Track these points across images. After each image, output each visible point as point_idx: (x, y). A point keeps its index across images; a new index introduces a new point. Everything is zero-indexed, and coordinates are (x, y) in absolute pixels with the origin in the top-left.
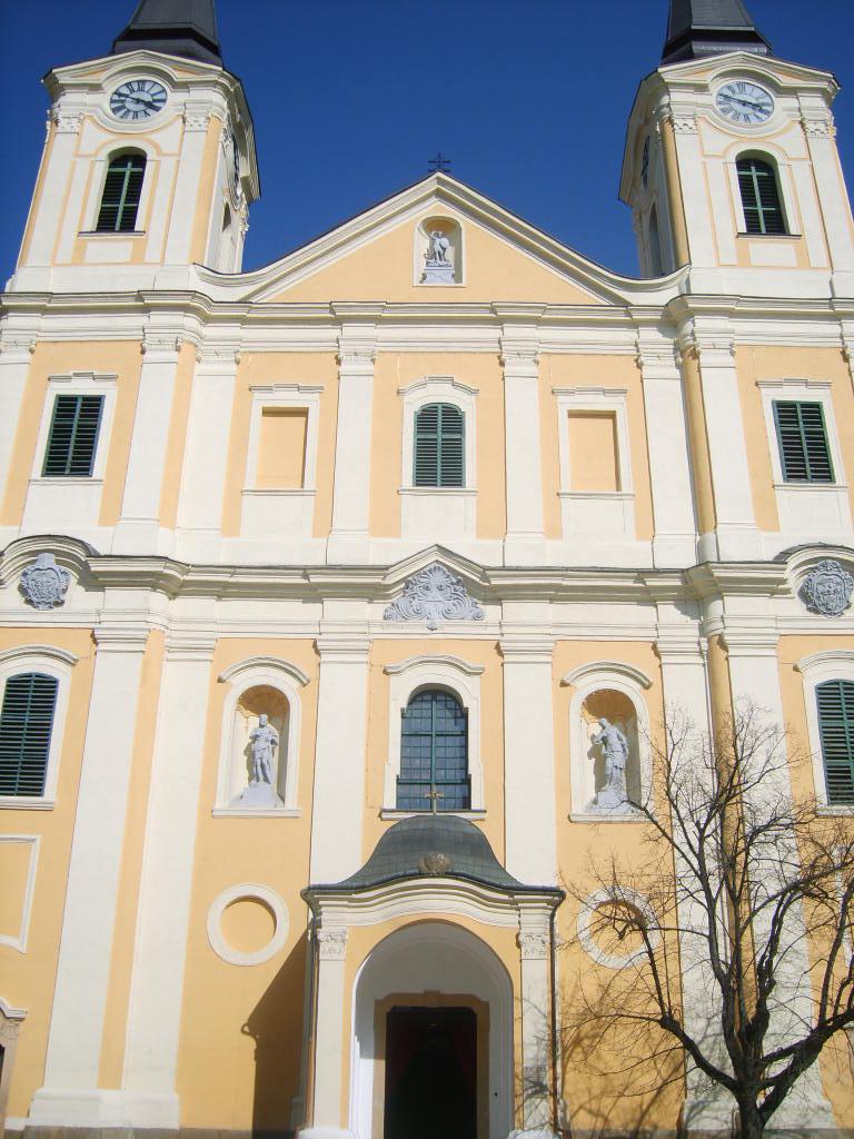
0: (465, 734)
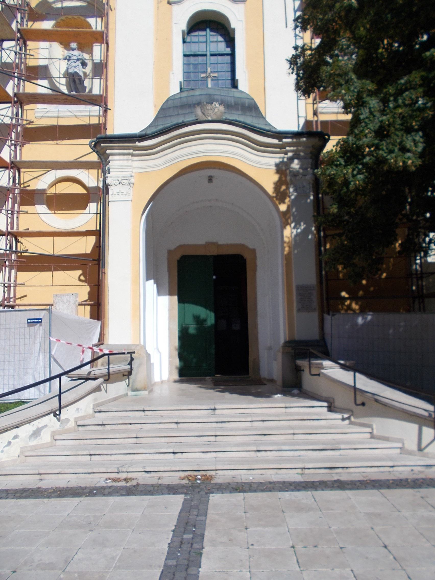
0: (233, 55)
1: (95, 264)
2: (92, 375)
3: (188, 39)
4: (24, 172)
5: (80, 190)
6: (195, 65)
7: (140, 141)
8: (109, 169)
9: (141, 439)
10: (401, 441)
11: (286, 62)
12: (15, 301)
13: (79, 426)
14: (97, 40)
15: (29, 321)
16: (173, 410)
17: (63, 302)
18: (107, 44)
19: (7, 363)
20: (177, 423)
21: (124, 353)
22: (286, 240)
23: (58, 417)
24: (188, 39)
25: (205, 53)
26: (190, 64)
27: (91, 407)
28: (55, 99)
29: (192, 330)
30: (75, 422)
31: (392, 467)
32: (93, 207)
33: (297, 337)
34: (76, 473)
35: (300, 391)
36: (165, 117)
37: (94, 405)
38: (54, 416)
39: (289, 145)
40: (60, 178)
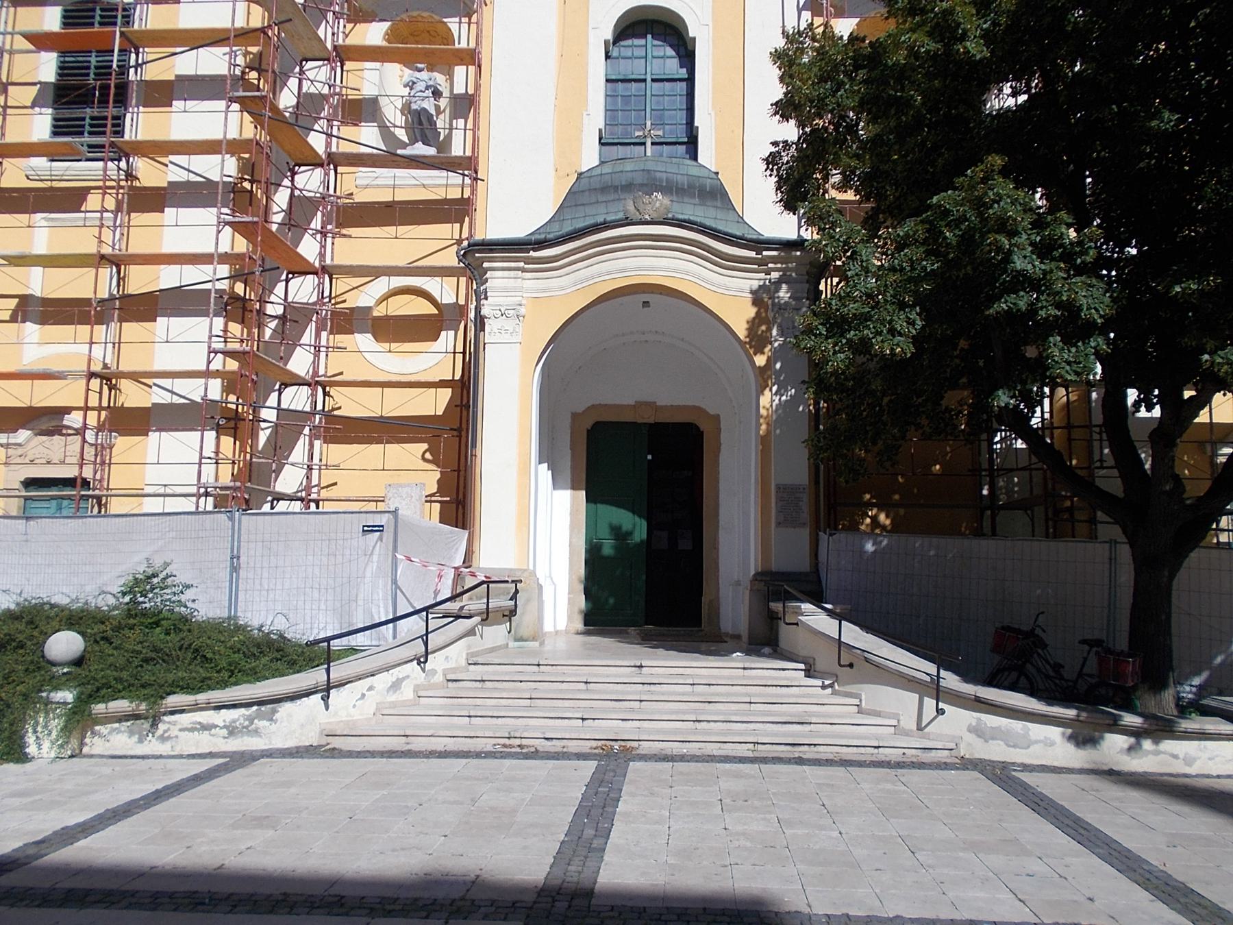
0: (690, 80)
1: (453, 436)
2: (465, 612)
3: (615, 52)
4: (337, 278)
5: (428, 309)
6: (626, 98)
7: (535, 250)
8: (486, 292)
9: (537, 701)
10: (896, 716)
11: (761, 161)
12: (319, 493)
13: (448, 680)
14: (462, 60)
15: (366, 528)
16: (558, 718)
17: (401, 496)
18: (480, 66)
19: (323, 591)
20: (586, 683)
21: (507, 582)
22: (763, 412)
23: (422, 665)
24: (615, 52)
25: (643, 77)
26: (617, 96)
27: (464, 656)
28: (393, 161)
29: (607, 550)
30: (414, 691)
32: (447, 339)
33: (774, 567)
34: (454, 737)
35: (775, 651)
36: (576, 205)
37: (467, 654)
38: (419, 664)
39: (774, 260)
40: (395, 288)
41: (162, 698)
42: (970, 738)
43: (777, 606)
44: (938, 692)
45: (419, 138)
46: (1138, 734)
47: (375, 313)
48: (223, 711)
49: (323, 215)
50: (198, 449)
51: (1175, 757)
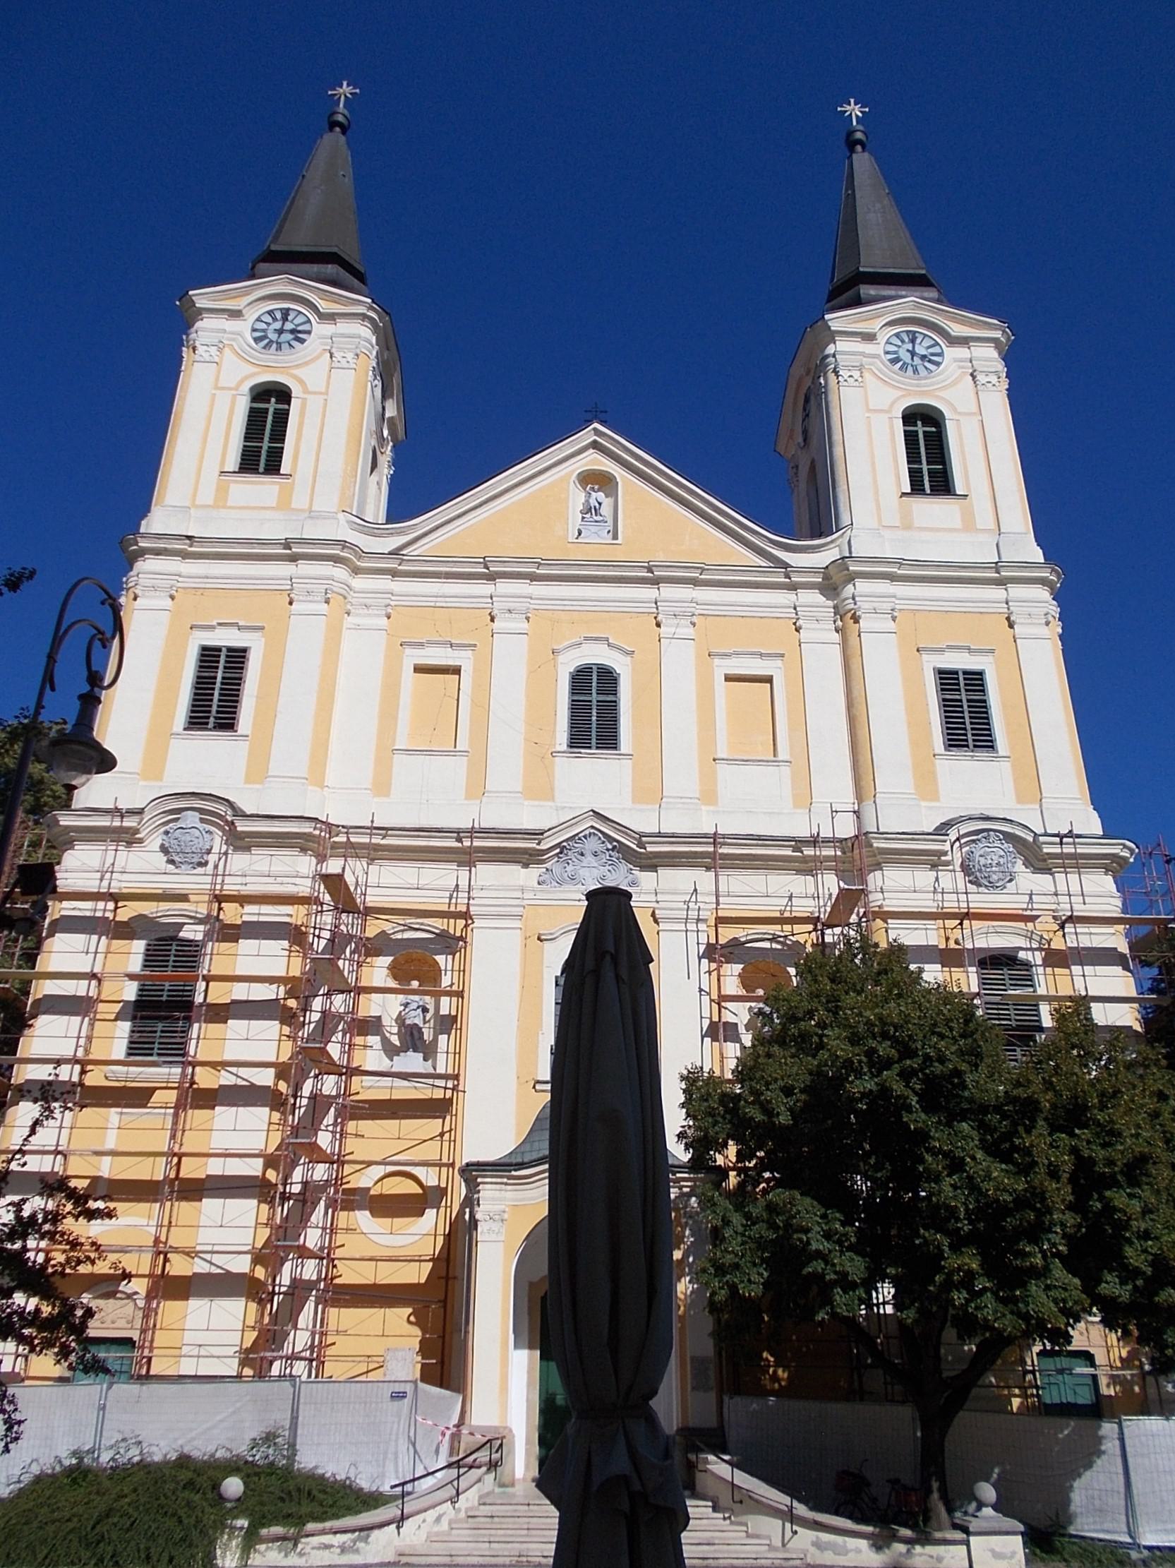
5: (415, 1189)
7: (515, 1170)
27: (477, 1498)
31: (756, 1559)
33: (691, 1425)
41: (304, 1525)
42: (813, 1549)
43: (692, 1457)
44: (790, 1517)
45: (410, 1045)
46: (909, 1541)
47: (372, 1192)
48: (338, 1535)
49: (336, 1110)
50: (242, 1318)
51: (932, 1557)
